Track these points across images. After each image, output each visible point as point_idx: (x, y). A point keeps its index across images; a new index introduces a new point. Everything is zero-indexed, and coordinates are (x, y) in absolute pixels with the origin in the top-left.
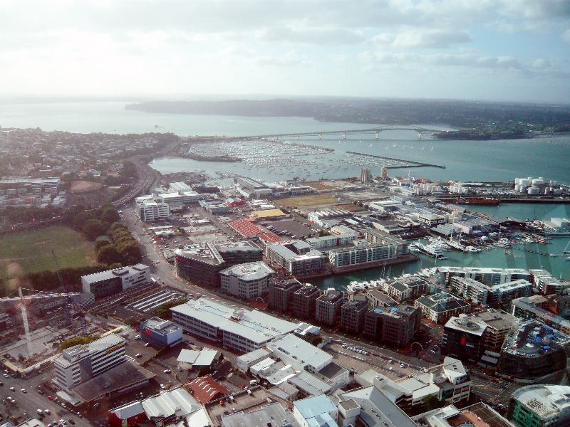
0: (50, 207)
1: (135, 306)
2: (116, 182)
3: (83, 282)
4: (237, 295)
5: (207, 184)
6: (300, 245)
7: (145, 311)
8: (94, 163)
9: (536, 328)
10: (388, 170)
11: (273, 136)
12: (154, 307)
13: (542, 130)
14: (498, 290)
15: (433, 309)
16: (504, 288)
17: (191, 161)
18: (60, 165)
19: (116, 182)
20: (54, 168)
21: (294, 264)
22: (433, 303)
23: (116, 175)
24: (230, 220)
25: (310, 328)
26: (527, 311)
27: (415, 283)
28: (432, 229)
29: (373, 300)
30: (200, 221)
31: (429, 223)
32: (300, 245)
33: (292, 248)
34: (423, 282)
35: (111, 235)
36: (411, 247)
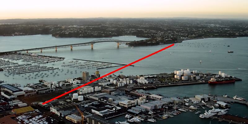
11: (24, 50)
13: (187, 36)
31: (127, 106)
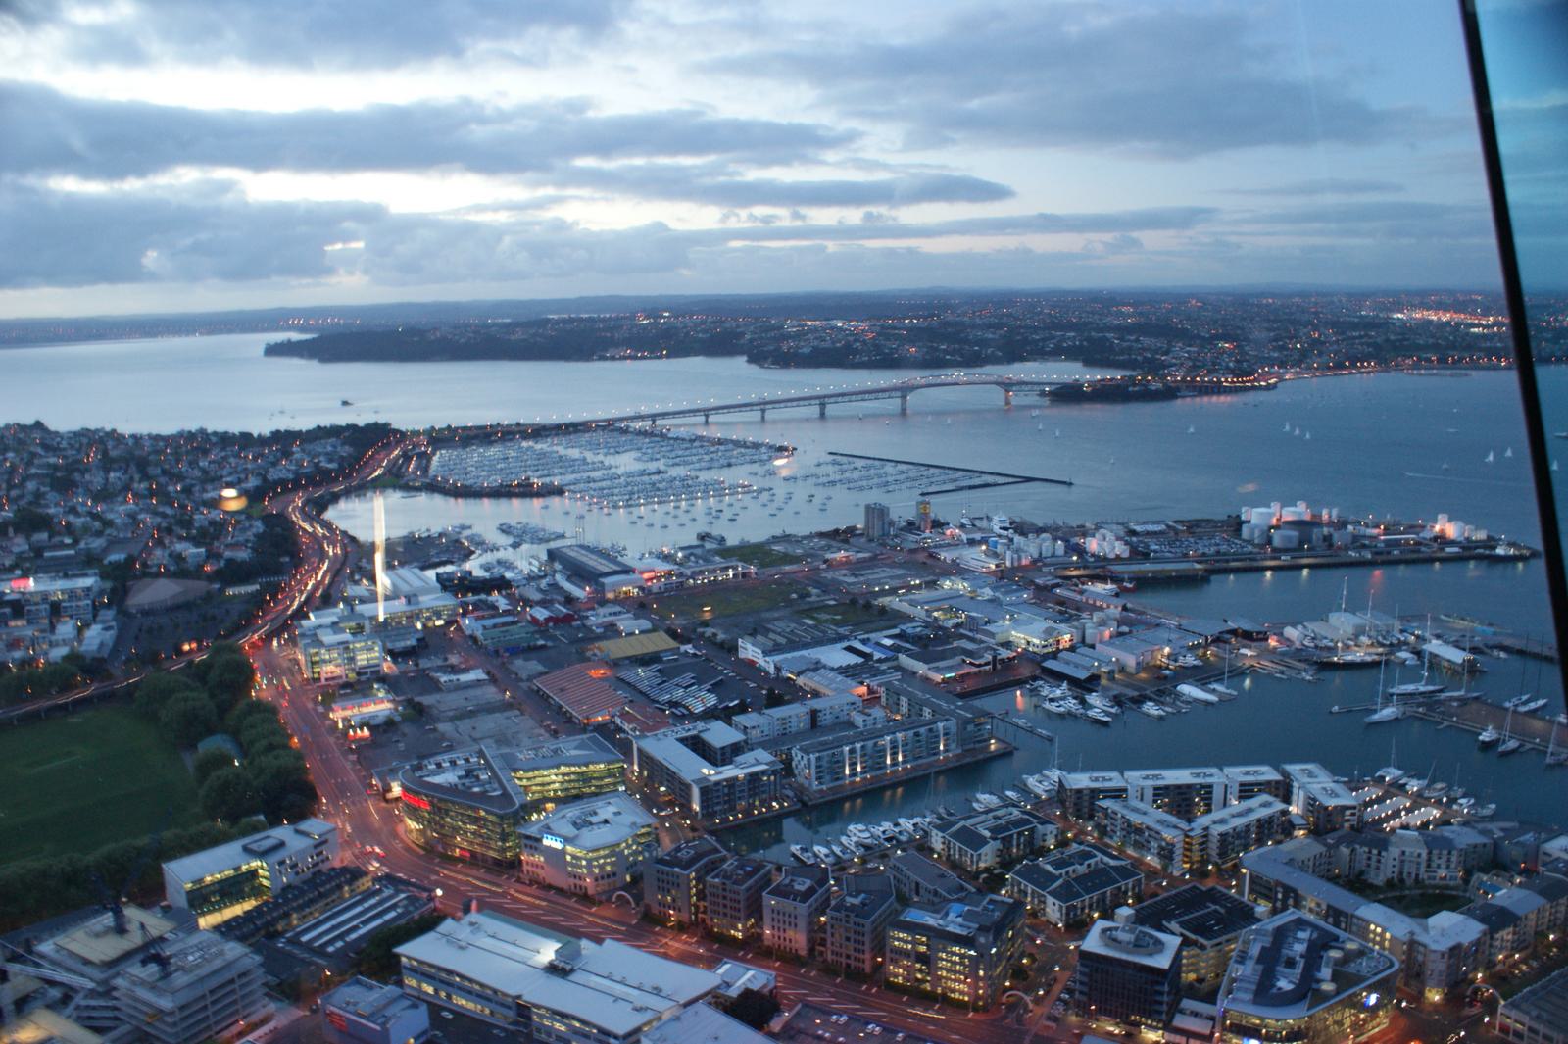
0: (73, 658)
1: (305, 939)
2: (235, 573)
3: (167, 878)
4: (566, 887)
5: (475, 566)
6: (719, 734)
7: (331, 949)
8: (187, 524)
9: (1301, 935)
10: (932, 499)
12: (354, 936)
14: (1206, 829)
15: (1052, 894)
16: (1222, 821)
17: (438, 500)
18: (99, 534)
19: (235, 573)
20: (82, 545)
21: (708, 791)
22: (1054, 878)
23: (243, 555)
24: (540, 668)
25: (748, 977)
26: (1278, 883)
27: (1005, 828)
28: (1045, 664)
29: (905, 880)
30: (464, 678)
32: (719, 734)
33: (697, 745)
34: (1028, 822)
35: (235, 734)
36: (1381, 315)
